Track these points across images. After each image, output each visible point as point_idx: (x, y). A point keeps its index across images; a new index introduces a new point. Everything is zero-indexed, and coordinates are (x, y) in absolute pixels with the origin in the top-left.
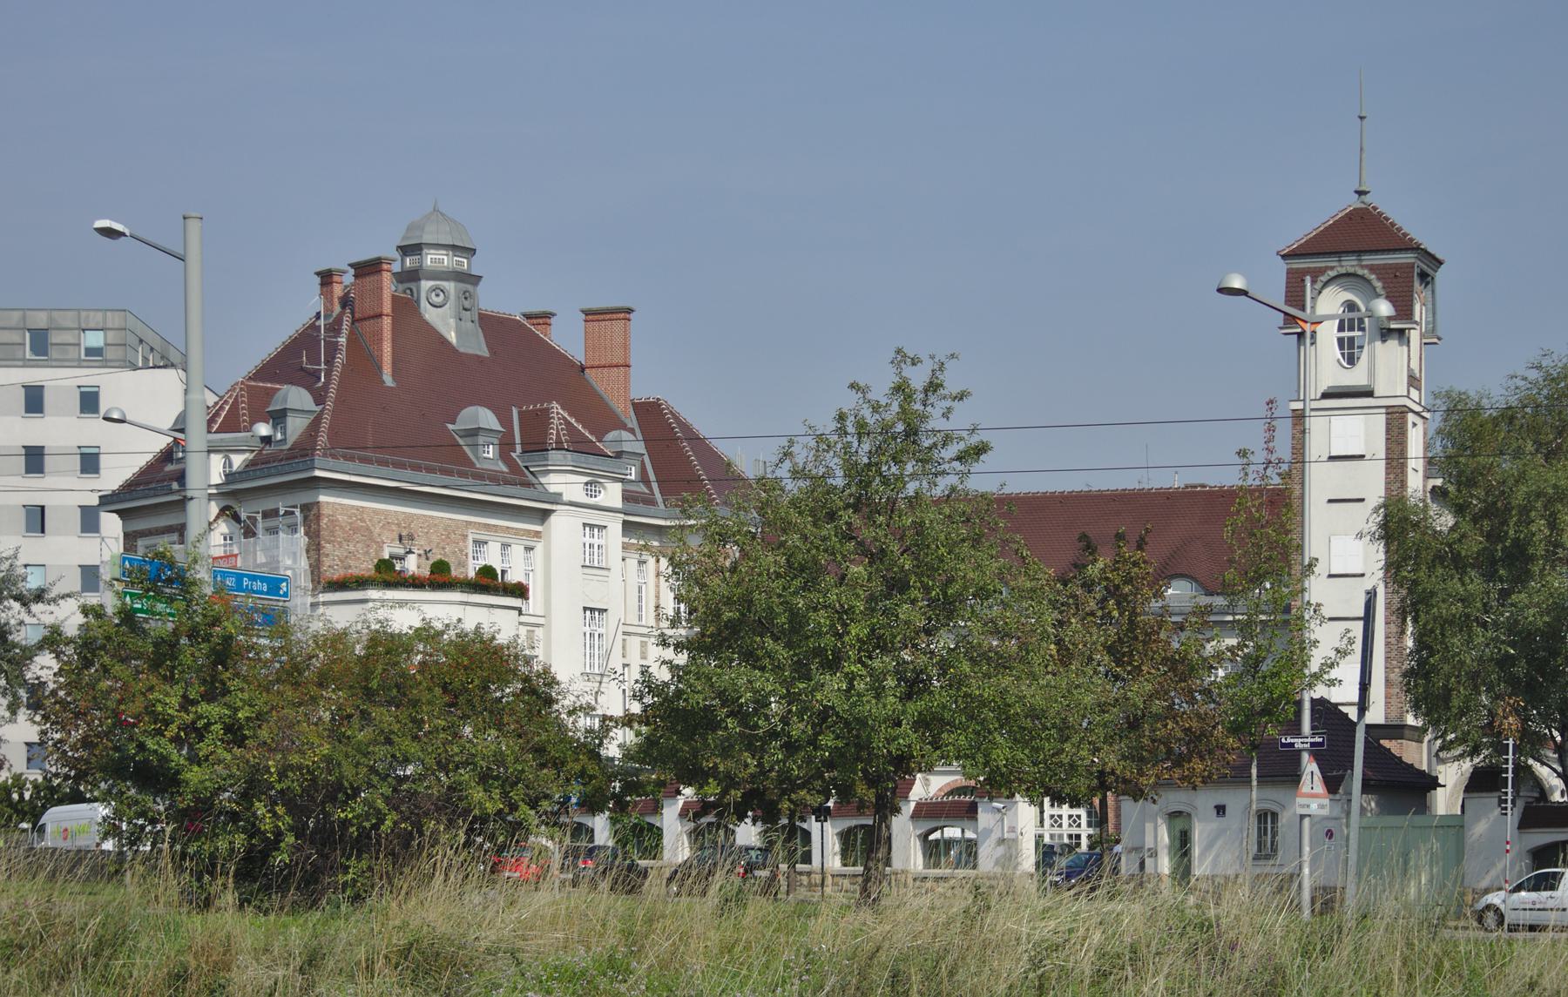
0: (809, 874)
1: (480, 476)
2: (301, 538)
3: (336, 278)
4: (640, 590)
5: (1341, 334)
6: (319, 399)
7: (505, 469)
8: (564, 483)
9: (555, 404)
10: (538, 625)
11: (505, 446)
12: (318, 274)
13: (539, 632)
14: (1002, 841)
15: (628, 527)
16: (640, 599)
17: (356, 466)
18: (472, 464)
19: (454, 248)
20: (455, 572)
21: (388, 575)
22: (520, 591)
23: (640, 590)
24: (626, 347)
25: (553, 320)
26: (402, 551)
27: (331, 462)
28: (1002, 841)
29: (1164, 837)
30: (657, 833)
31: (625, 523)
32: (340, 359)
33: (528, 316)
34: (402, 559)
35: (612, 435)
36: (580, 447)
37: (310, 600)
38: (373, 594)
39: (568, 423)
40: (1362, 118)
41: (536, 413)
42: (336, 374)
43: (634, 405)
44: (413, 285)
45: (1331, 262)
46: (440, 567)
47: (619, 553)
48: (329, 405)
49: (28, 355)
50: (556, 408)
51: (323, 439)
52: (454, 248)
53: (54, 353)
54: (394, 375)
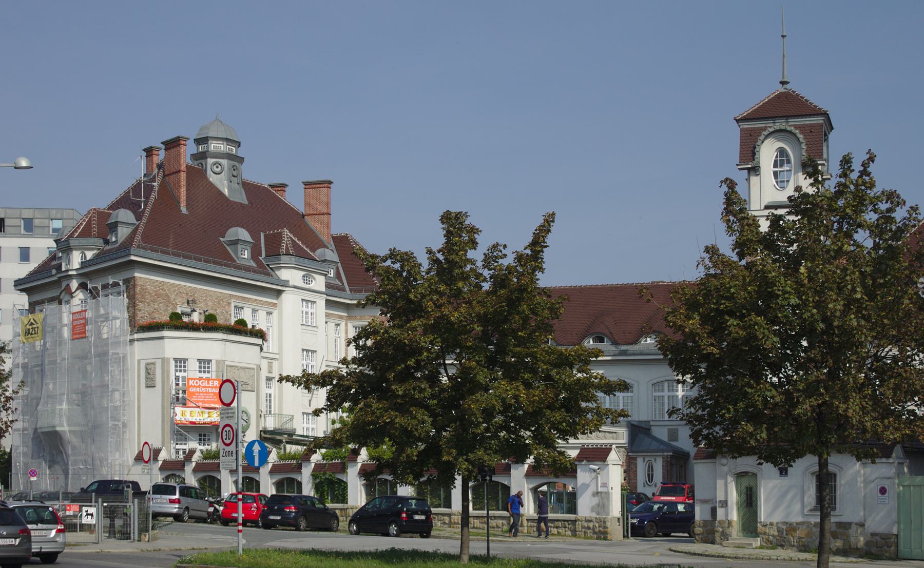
0: (449, 515)
1: (239, 267)
2: (124, 300)
3: (155, 152)
4: (336, 341)
5: (776, 169)
6: (139, 217)
7: (254, 265)
8: (291, 275)
9: (285, 230)
10: (275, 359)
11: (255, 255)
12: (144, 150)
13: (275, 363)
14: (597, 494)
15: (328, 302)
16: (336, 346)
18: (234, 261)
19: (227, 140)
20: (220, 321)
21: (177, 323)
22: (261, 335)
23: (336, 341)
24: (328, 203)
25: (286, 189)
26: (189, 310)
27: (142, 252)
28: (597, 494)
29: (733, 496)
30: (343, 486)
31: (327, 301)
32: (154, 195)
33: (272, 186)
34: (189, 315)
35: (320, 251)
36: (300, 254)
37: (129, 338)
38: (166, 333)
39: (293, 241)
40: (783, 36)
41: (274, 235)
42: (150, 204)
43: (333, 238)
44: (203, 162)
45: (769, 123)
47: (323, 319)
48: (144, 220)
49: (23, 231)
50: (286, 232)
51: (138, 238)
52: (227, 140)
53: (36, 230)
54: (188, 207)
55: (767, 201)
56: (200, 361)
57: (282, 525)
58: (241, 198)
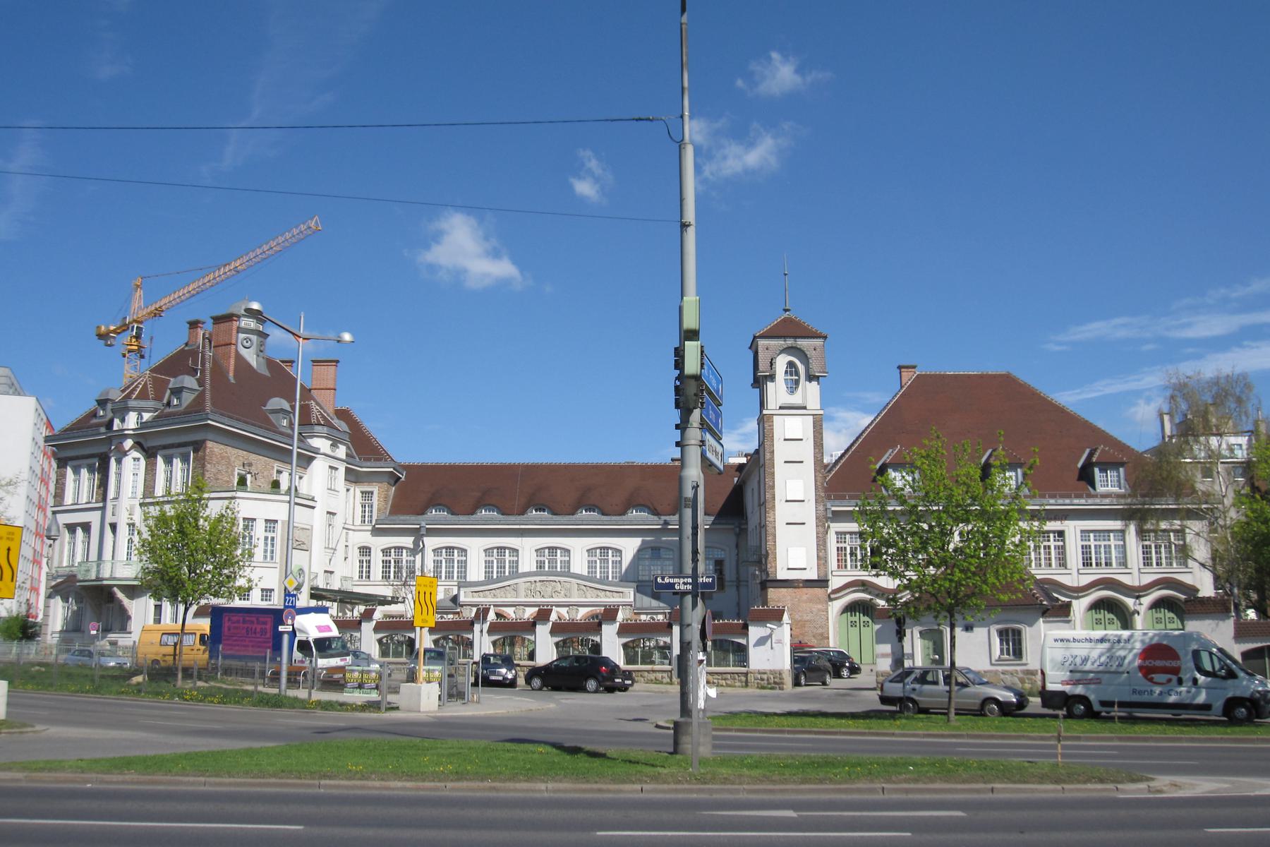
17: (226, 420)
42: (208, 372)
46: (678, 444)
48: (208, 386)
54: (235, 376)
55: (781, 402)
56: (267, 521)
57: (8, 728)
58: (264, 371)
